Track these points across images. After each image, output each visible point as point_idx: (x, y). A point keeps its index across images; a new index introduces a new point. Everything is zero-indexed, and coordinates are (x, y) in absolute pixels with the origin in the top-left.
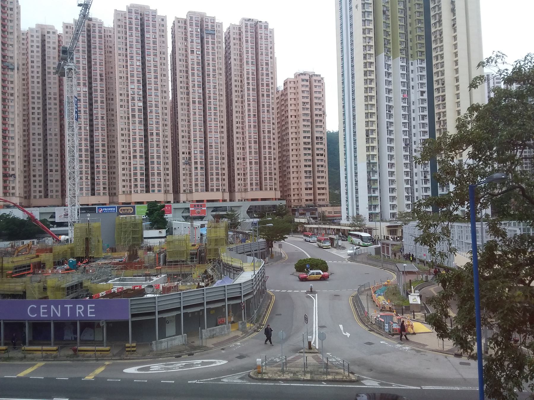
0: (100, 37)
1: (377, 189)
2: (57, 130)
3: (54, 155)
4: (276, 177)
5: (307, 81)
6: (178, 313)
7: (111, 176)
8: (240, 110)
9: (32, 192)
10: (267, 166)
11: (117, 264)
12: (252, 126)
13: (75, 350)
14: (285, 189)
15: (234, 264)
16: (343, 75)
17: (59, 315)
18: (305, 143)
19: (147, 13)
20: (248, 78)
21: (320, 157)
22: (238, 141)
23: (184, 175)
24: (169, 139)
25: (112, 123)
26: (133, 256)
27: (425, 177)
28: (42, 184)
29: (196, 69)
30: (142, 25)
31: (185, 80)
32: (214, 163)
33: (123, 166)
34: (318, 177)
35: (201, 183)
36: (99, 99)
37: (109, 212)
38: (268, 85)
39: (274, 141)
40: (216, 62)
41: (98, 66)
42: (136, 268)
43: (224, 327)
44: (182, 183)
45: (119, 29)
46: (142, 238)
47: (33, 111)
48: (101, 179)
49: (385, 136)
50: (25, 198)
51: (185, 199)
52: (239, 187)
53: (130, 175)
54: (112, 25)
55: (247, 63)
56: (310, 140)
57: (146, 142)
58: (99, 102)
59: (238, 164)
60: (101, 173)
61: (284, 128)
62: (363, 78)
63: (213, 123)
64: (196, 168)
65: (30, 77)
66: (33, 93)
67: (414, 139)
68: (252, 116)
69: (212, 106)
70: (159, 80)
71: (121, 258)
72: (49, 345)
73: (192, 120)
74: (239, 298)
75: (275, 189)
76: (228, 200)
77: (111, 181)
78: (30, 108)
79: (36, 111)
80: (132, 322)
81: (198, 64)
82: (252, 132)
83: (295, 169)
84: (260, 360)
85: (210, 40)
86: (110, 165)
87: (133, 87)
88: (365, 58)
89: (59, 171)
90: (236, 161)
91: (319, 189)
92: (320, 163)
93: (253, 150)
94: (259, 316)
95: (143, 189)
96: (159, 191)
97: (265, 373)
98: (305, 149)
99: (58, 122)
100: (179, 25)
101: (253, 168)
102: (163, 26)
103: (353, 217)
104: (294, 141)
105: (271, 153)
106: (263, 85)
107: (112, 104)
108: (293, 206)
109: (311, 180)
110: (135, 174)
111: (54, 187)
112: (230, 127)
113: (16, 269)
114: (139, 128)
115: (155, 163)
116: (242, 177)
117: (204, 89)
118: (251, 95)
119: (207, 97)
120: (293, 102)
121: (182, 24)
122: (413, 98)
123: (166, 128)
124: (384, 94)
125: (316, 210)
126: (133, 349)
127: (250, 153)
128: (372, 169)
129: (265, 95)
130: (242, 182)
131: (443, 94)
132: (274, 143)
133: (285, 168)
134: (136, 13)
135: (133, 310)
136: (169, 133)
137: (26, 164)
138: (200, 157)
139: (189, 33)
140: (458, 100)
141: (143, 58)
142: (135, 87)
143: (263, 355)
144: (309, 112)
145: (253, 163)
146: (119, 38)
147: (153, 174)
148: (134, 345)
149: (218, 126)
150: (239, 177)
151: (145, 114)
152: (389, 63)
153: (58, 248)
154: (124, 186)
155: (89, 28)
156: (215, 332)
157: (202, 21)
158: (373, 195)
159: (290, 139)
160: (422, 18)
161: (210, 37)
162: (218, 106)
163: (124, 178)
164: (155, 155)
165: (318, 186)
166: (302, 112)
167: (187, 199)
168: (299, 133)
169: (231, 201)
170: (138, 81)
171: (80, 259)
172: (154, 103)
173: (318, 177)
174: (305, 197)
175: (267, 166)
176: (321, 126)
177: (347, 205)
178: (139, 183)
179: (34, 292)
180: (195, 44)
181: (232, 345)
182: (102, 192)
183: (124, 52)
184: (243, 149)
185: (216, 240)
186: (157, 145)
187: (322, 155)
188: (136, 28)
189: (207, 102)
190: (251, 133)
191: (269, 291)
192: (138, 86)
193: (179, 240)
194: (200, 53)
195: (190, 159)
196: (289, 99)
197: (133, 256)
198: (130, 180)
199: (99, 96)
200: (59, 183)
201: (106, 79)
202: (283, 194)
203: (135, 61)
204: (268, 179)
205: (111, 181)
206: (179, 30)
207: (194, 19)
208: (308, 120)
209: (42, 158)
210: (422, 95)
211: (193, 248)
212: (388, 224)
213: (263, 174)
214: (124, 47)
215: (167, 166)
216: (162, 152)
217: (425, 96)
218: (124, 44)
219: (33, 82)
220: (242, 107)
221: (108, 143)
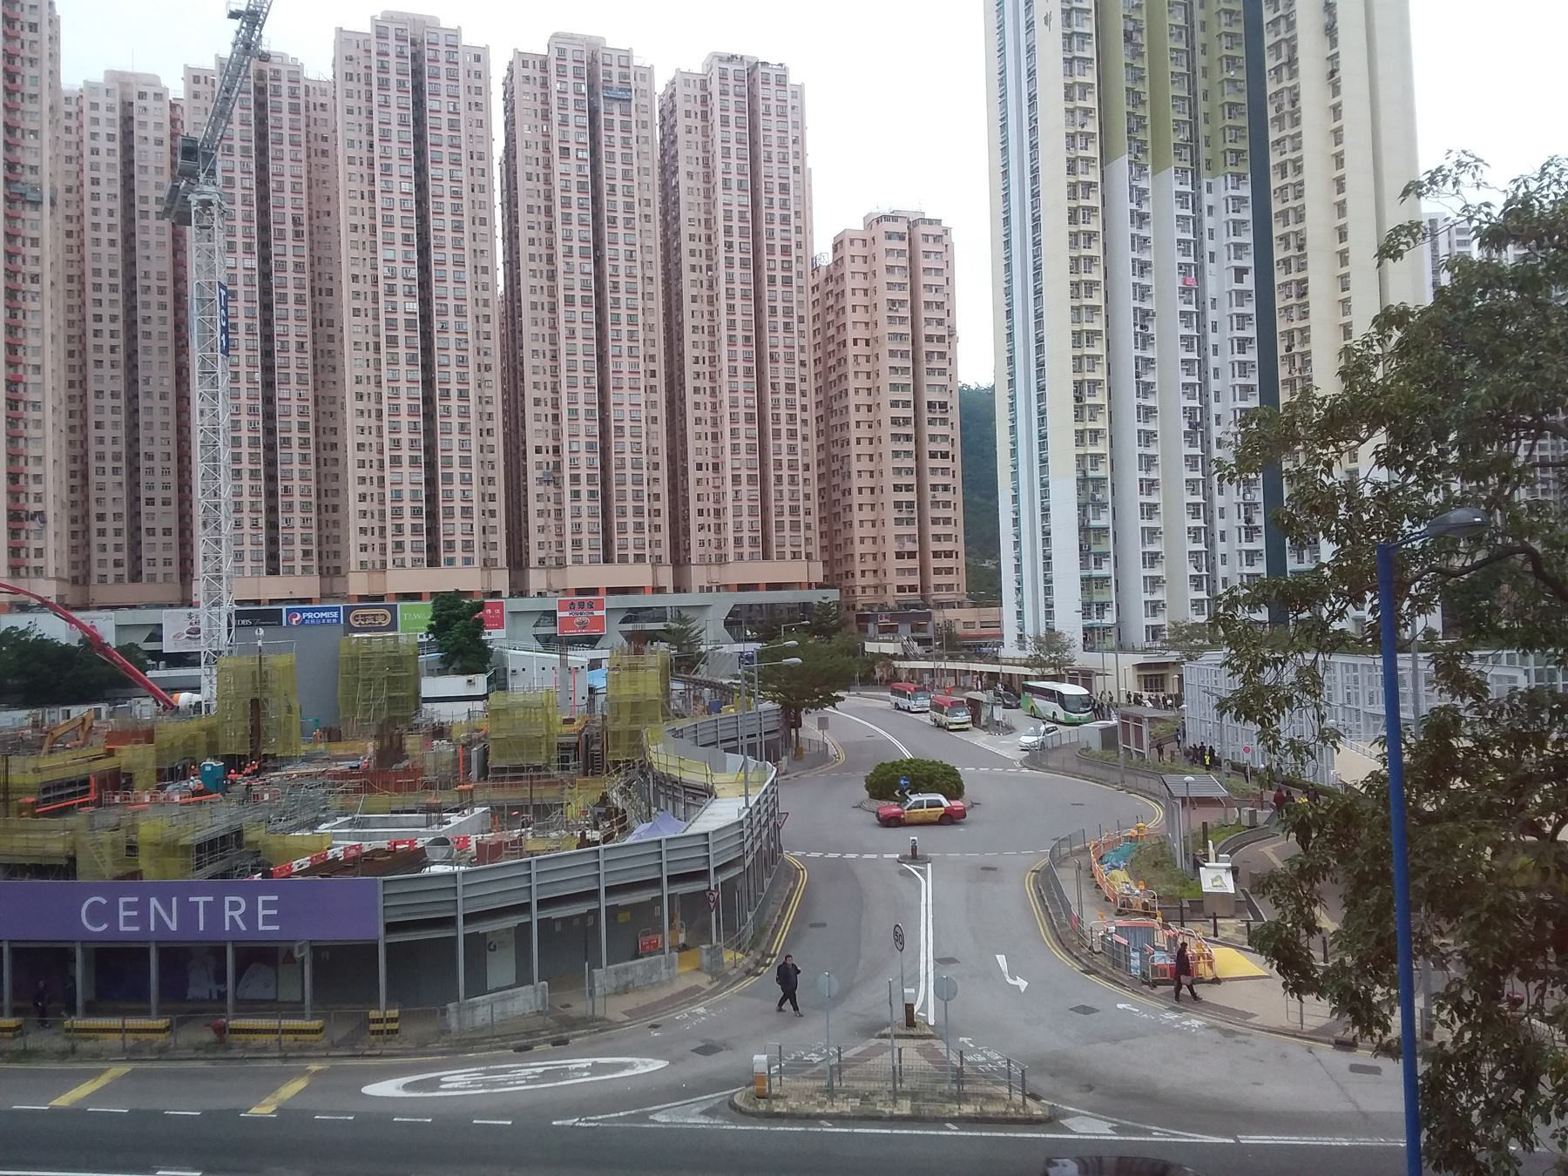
0: (294, 109)
1: (1106, 555)
2: (166, 382)
3: (157, 457)
4: (809, 519)
5: (902, 238)
6: (524, 919)
7: (325, 516)
8: (706, 324)
9: (94, 563)
10: (785, 487)
11: (345, 775)
12: (740, 372)
13: (221, 1030)
14: (838, 556)
15: (688, 777)
16: (1007, 221)
17: (173, 926)
18: (895, 421)
19: (433, 38)
20: (728, 230)
21: (939, 463)
22: (698, 413)
23: (540, 513)
24: (497, 408)
25: (330, 361)
26: (391, 752)
27: (1248, 520)
28: (123, 540)
29: (574, 203)
30: (417, 73)
31: (543, 235)
32: (629, 480)
33: (362, 489)
34: (935, 521)
35: (590, 539)
36: (291, 292)
37: (321, 623)
38: (786, 250)
39: (806, 416)
40: (636, 184)
41: (288, 194)
42: (398, 789)
43: (659, 961)
44: (534, 537)
45: (350, 86)
46: (418, 700)
47: (98, 326)
48: (297, 525)
49: (1130, 400)
50: (75, 581)
51: (543, 586)
52: (702, 551)
53: (382, 514)
54: (328, 75)
55: (726, 185)
56: (909, 413)
57: (429, 416)
58: (291, 299)
59: (699, 481)
60: (297, 507)
61: (833, 376)
62: (1066, 228)
63: (625, 362)
64: (576, 495)
65: (87, 227)
66: (97, 272)
67: (1215, 408)
68: (740, 340)
69: (624, 312)
70: (467, 235)
71: (355, 757)
72: (145, 1013)
73: (563, 352)
74: (702, 875)
75: (808, 556)
76: (670, 589)
77: (325, 532)
78: (89, 318)
79: (106, 326)
80: (388, 946)
81: (581, 187)
82: (741, 389)
83: (866, 497)
84: (764, 1057)
85: (617, 118)
86: (324, 486)
87: (390, 255)
88: (1071, 169)
89: (175, 501)
90: (693, 474)
91: (936, 554)
92: (939, 480)
93: (743, 442)
94: (761, 930)
95: (420, 555)
96: (468, 561)
97: (777, 1097)
98: (896, 437)
99: (170, 357)
100: (526, 72)
101: (744, 495)
102: (478, 75)
103: (1037, 639)
104: (863, 415)
105: (797, 449)
106: (771, 249)
107: (330, 306)
108: (859, 607)
109: (914, 530)
110: (397, 513)
111: (159, 549)
112: (677, 373)
113: (46, 790)
114: (407, 377)
115: (457, 479)
116: (712, 521)
117: (598, 262)
118: (737, 279)
119: (608, 285)
120: (860, 299)
121: (533, 72)
122: (1212, 288)
123: (487, 376)
124: (1127, 278)
125: (928, 617)
126: (390, 1026)
127: (735, 449)
128: (1093, 497)
129: (779, 280)
130: (712, 535)
131: (1300, 276)
132: (804, 422)
133: (837, 495)
134: (398, 38)
135: (391, 912)
136: (495, 391)
137: (77, 481)
138: (587, 462)
139: (555, 96)
140: (1346, 295)
141: (421, 170)
142: (397, 256)
143: (773, 1043)
144: (906, 329)
145: (744, 479)
146: (350, 112)
147: (449, 513)
148: (394, 1013)
149: (641, 370)
150: (701, 520)
151: (426, 336)
152: (1143, 184)
153: (170, 729)
154: (364, 548)
155: (260, 84)
156: (630, 977)
157: (593, 61)
158: (1096, 573)
159: (852, 409)
160: (1240, 52)
161: (616, 108)
162: (640, 312)
163: (364, 523)
164: (456, 455)
165: (934, 546)
166: (885, 329)
167: (549, 584)
168: (877, 391)
169: (677, 590)
170: (406, 237)
171: (234, 762)
172: (451, 303)
173: (935, 521)
174: (895, 580)
175: (785, 487)
176: (942, 372)
177: (1020, 604)
178: (407, 538)
179: (100, 860)
180: (572, 129)
181: (682, 1015)
182: (299, 563)
183: (365, 154)
184: (715, 437)
185: (635, 706)
186: (462, 427)
187: (945, 455)
188: (401, 84)
189: (609, 301)
190: (736, 390)
191: (791, 856)
192: (406, 252)
193: (526, 707)
194: (586, 155)
195: (557, 466)
196: (848, 292)
197: (391, 752)
198: (382, 529)
199: (291, 283)
200: (174, 539)
201: (311, 234)
202: (832, 571)
203: (396, 179)
204: (787, 526)
205: (325, 532)
206: (527, 88)
207: (569, 56)
208: (904, 354)
209: (123, 464)
210: (1239, 280)
211: (566, 729)
212: (1140, 659)
213: (773, 510)
214: (365, 138)
215: (491, 489)
216: (474, 447)
217: (1249, 282)
218: (364, 128)
219: (97, 242)
220: (711, 314)
221: (317, 420)
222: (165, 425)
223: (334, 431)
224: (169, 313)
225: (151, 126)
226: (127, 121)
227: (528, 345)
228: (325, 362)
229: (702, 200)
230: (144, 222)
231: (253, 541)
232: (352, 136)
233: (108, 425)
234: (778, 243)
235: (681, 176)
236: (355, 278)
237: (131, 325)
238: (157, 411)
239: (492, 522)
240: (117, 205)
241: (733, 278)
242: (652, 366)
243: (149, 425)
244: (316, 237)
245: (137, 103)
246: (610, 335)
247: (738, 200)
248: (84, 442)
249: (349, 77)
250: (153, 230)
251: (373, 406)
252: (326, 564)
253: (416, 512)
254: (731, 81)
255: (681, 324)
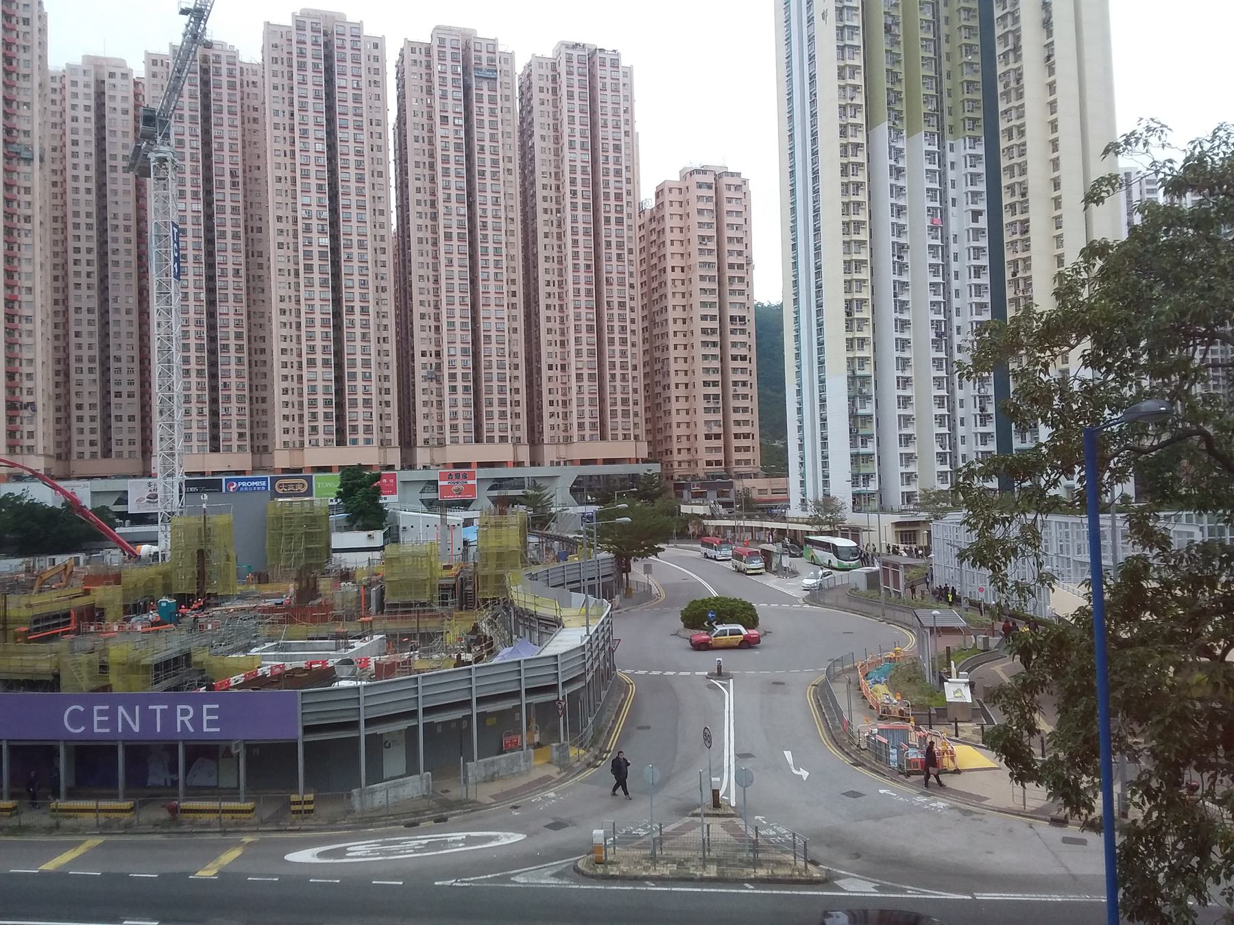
0: (232, 86)
1: (871, 436)
2: (131, 300)
3: (124, 360)
4: (637, 408)
5: (710, 187)
6: (412, 723)
7: (256, 406)
8: (556, 255)
9: (74, 443)
10: (618, 383)
11: (271, 610)
12: (583, 292)
13: (174, 810)
14: (659, 437)
15: (541, 611)
16: (792, 173)
17: (136, 729)
18: (704, 331)
19: (341, 30)
20: (573, 181)
21: (739, 364)
22: (549, 325)
23: (425, 404)
24: (391, 321)
25: (260, 284)
26: (308, 591)
27: (982, 409)
28: (97, 425)
29: (452, 160)
30: (328, 57)
31: (428, 185)
32: (495, 378)
33: (285, 385)
34: (736, 410)
35: (464, 424)
36: (229, 230)
37: (253, 490)
38: (618, 197)
39: (634, 327)
40: (500, 144)
41: (226, 153)
42: (313, 620)
43: (519, 756)
44: (421, 423)
45: (276, 67)
46: (329, 551)
47: (77, 256)
48: (234, 413)
49: (890, 315)
50: (59, 457)
51: (427, 461)
52: (552, 433)
53: (301, 404)
54: (258, 59)
55: (572, 146)
56: (716, 325)
57: (338, 328)
58: (229, 235)
59: (550, 379)
60: (234, 399)
61: (656, 296)
62: (839, 179)
63: (492, 285)
64: (453, 389)
65: (69, 178)
66: (76, 214)
67: (956, 321)
68: (582, 268)
69: (491, 246)
70: (367, 185)
71: (280, 596)
72: (114, 797)
73: (443, 277)
74: (552, 688)
75: (636, 437)
76: (527, 463)
77: (256, 419)
78: (70, 251)
79: (84, 256)
80: (306, 744)
81: (458, 147)
82: (583, 306)
83: (682, 391)
84: (602, 832)
85: (486, 93)
86: (255, 382)
87: (307, 201)
88: (843, 133)
89: (137, 394)
90: (545, 373)
91: (737, 436)
92: (739, 377)
93: (585, 347)
94: (599, 731)
95: (330, 437)
96: (368, 441)
97: (611, 863)
98: (705, 344)
99: (134, 281)
100: (414, 57)
101: (586, 389)
102: (376, 59)
103: (816, 502)
104: (679, 326)
105: (627, 353)
106: (607, 195)
107: (260, 241)
108: (676, 477)
109: (719, 417)
110: (313, 403)
111: (125, 432)
112: (533, 293)
113: (36, 622)
114: (320, 297)
115: (359, 377)
116: (560, 409)
117: (471, 206)
118: (580, 219)
119: (479, 224)
120: (676, 235)
121: (420, 57)
122: (954, 227)
123: (384, 295)
124: (887, 218)
125: (731, 485)
126: (307, 807)
127: (578, 353)
128: (860, 391)
129: (613, 221)
130: (560, 421)
131: (1023, 217)
132: (633, 332)
133: (658, 390)
134: (313, 30)
135: (308, 717)
136: (390, 308)
137: (61, 379)
138: (462, 364)
139: (436, 75)
140: (1059, 232)
141: (331, 134)
142: (312, 202)
143: (609, 820)
144: (713, 259)
145: (586, 377)
146: (276, 88)
147: (354, 403)
148: (310, 797)
149: (505, 291)
150: (552, 409)
151: (336, 264)
152: (899, 145)
153: (134, 574)
154: (286, 431)
155: (205, 66)
156: (496, 769)
157: (467, 48)
158: (862, 451)
159: (671, 321)
160: (976, 41)
161: (485, 85)
162: (504, 245)
163: (286, 411)
164: (359, 358)
165: (735, 430)
166: (697, 259)
167: (432, 460)
168: (690, 307)
169: (533, 464)
170: (320, 187)
171: (184, 600)
172: (355, 238)
173: (736, 410)
174: (704, 456)
175: (618, 383)
176: (741, 292)
177: (803, 475)
178: (321, 423)
179: (78, 676)
180: (450, 101)
181: (537, 798)
182: (235, 443)
183: (287, 121)
184: (563, 344)
185: (500, 555)
186: (364, 335)
187: (744, 358)
188: (315, 66)
189: (479, 237)
190: (579, 307)
191: (622, 673)
192: (320, 199)
193: (414, 556)
194: (461, 122)
195: (439, 367)
196: (668, 230)
197: (308, 591)
198: (301, 416)
199: (229, 223)
200: (137, 424)
201: (245, 184)
202: (655, 449)
203: (311, 141)
204: (619, 414)
205: (256, 419)
206: (415, 69)
207: (448, 44)
208: (711, 279)
209: (96, 365)
210: (975, 220)
211: (446, 573)
212: (897, 518)
213: (608, 401)
214: (287, 109)
215: (386, 385)
216: (373, 352)
217: (983, 222)
218: (287, 101)
219: (76, 190)
220: (560, 247)
221: (249, 331)
222: (130, 334)
223: (263, 339)
224: (133, 246)
225: (119, 99)
226: (100, 95)
227: (416, 271)
228: (255, 285)
229: (552, 158)
230: (114, 175)
231: (199, 425)
232: (277, 107)
233: (85, 334)
234: (612, 191)
235: (536, 139)
236: (279, 219)
237: (103, 255)
238: (123, 323)
239: (388, 410)
240: (92, 161)
241: (577, 219)
242: (513, 288)
243: (118, 334)
244: (249, 187)
245: (108, 81)
246: (480, 263)
247: (581, 157)
248: (66, 348)
249: (275, 60)
250: (120, 181)
251: (294, 319)
252: (256, 443)
253: (327, 403)
254: (575, 64)
255: (536, 255)
